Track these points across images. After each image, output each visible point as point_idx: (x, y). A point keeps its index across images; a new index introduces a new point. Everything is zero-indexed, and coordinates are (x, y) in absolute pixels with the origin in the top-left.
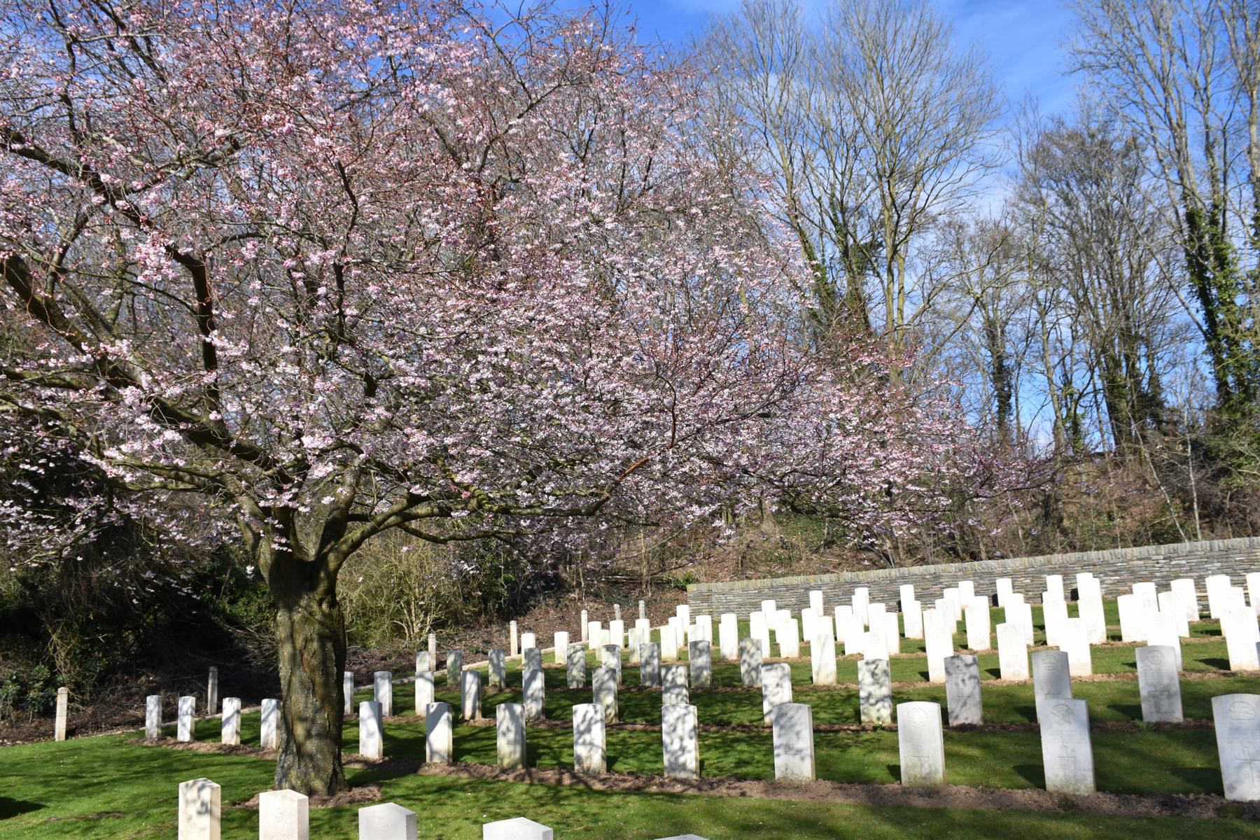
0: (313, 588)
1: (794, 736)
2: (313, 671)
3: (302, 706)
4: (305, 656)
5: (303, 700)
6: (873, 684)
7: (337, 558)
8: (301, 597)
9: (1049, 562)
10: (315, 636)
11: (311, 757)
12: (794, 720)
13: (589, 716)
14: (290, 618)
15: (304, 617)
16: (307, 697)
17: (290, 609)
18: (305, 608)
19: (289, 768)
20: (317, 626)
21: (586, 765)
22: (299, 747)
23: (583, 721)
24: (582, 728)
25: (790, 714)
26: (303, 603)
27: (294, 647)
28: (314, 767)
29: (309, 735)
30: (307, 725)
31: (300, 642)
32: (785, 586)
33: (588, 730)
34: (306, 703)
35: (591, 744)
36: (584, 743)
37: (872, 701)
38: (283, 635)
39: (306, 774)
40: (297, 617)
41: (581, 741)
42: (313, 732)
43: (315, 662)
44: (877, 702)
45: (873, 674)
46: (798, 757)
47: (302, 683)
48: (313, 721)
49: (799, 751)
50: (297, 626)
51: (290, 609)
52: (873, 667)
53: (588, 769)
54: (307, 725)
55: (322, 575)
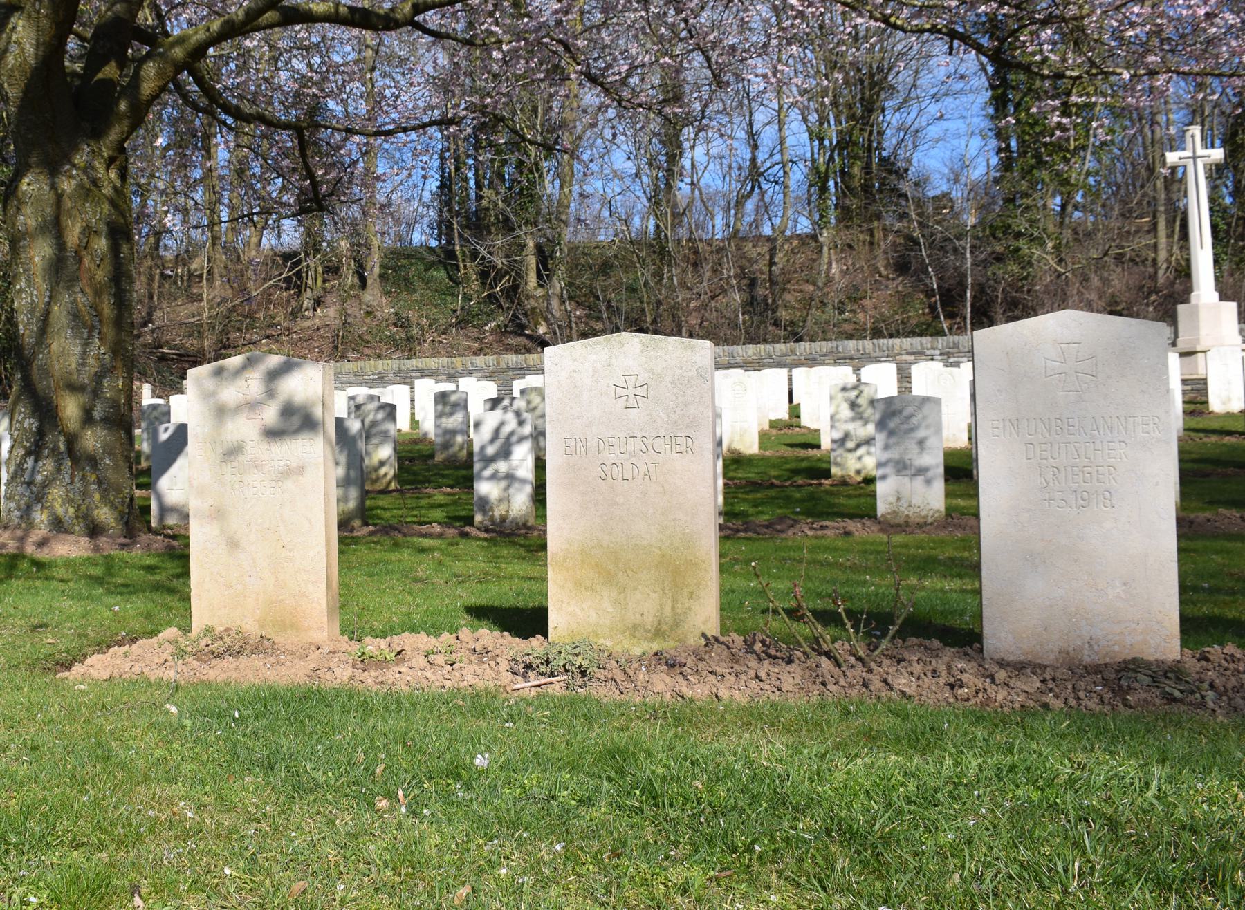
0: (97, 134)
1: (914, 448)
2: (98, 293)
3: (73, 363)
4: (86, 261)
5: (77, 350)
6: (853, 419)
7: (160, 73)
8: (75, 148)
9: (793, 352)
10: (103, 227)
11: (93, 461)
12: (914, 421)
13: (506, 430)
14: (53, 187)
15: (81, 186)
16: (86, 344)
17: (53, 168)
18: (85, 171)
19: (47, 484)
20: (106, 207)
21: (498, 512)
22: (71, 440)
23: (492, 441)
24: (490, 450)
25: (906, 413)
26: (80, 159)
27: (61, 245)
28: (99, 482)
29: (87, 418)
30: (83, 399)
31: (73, 236)
32: (417, 370)
33: (505, 453)
34: (84, 355)
35: (510, 477)
36: (494, 477)
37: (850, 445)
38: (32, 223)
39: (85, 494)
40: (67, 186)
41: (487, 473)
42: (97, 414)
43: (101, 275)
44: (858, 446)
45: (853, 405)
46: (919, 480)
47: (75, 315)
48: (96, 393)
49: (922, 471)
50: (68, 204)
51: (53, 168)
52: (853, 394)
53: (503, 519)
54: (83, 399)
55: (123, 106)
